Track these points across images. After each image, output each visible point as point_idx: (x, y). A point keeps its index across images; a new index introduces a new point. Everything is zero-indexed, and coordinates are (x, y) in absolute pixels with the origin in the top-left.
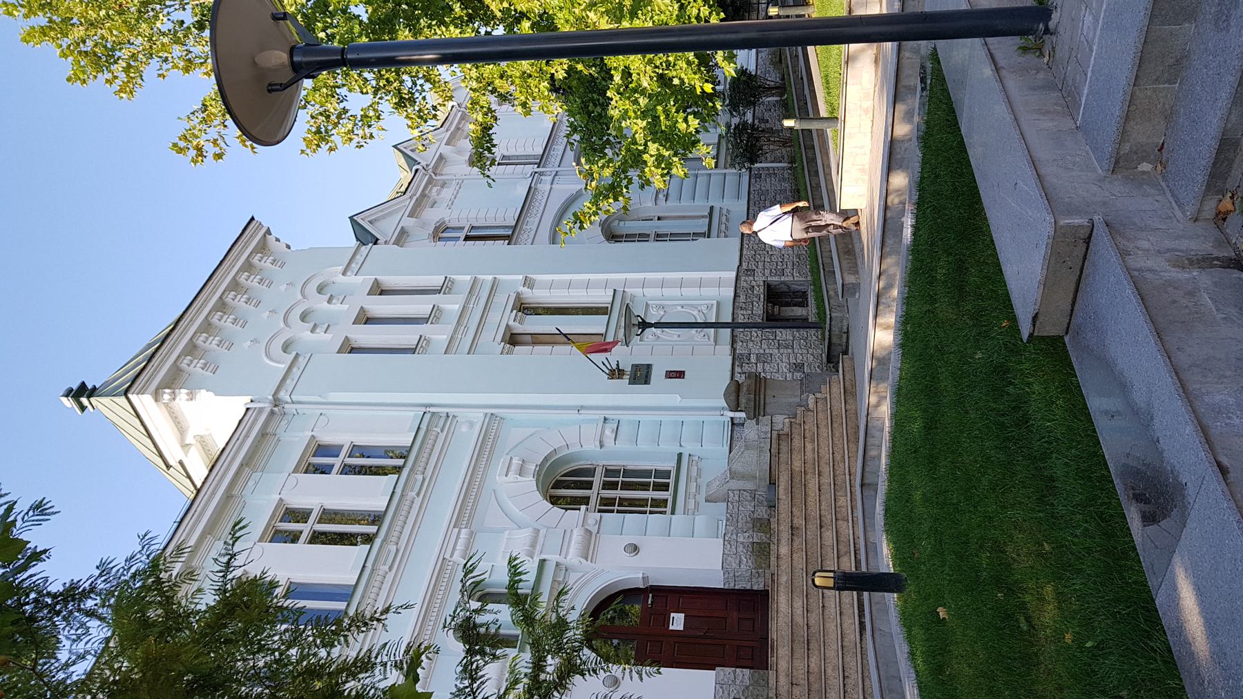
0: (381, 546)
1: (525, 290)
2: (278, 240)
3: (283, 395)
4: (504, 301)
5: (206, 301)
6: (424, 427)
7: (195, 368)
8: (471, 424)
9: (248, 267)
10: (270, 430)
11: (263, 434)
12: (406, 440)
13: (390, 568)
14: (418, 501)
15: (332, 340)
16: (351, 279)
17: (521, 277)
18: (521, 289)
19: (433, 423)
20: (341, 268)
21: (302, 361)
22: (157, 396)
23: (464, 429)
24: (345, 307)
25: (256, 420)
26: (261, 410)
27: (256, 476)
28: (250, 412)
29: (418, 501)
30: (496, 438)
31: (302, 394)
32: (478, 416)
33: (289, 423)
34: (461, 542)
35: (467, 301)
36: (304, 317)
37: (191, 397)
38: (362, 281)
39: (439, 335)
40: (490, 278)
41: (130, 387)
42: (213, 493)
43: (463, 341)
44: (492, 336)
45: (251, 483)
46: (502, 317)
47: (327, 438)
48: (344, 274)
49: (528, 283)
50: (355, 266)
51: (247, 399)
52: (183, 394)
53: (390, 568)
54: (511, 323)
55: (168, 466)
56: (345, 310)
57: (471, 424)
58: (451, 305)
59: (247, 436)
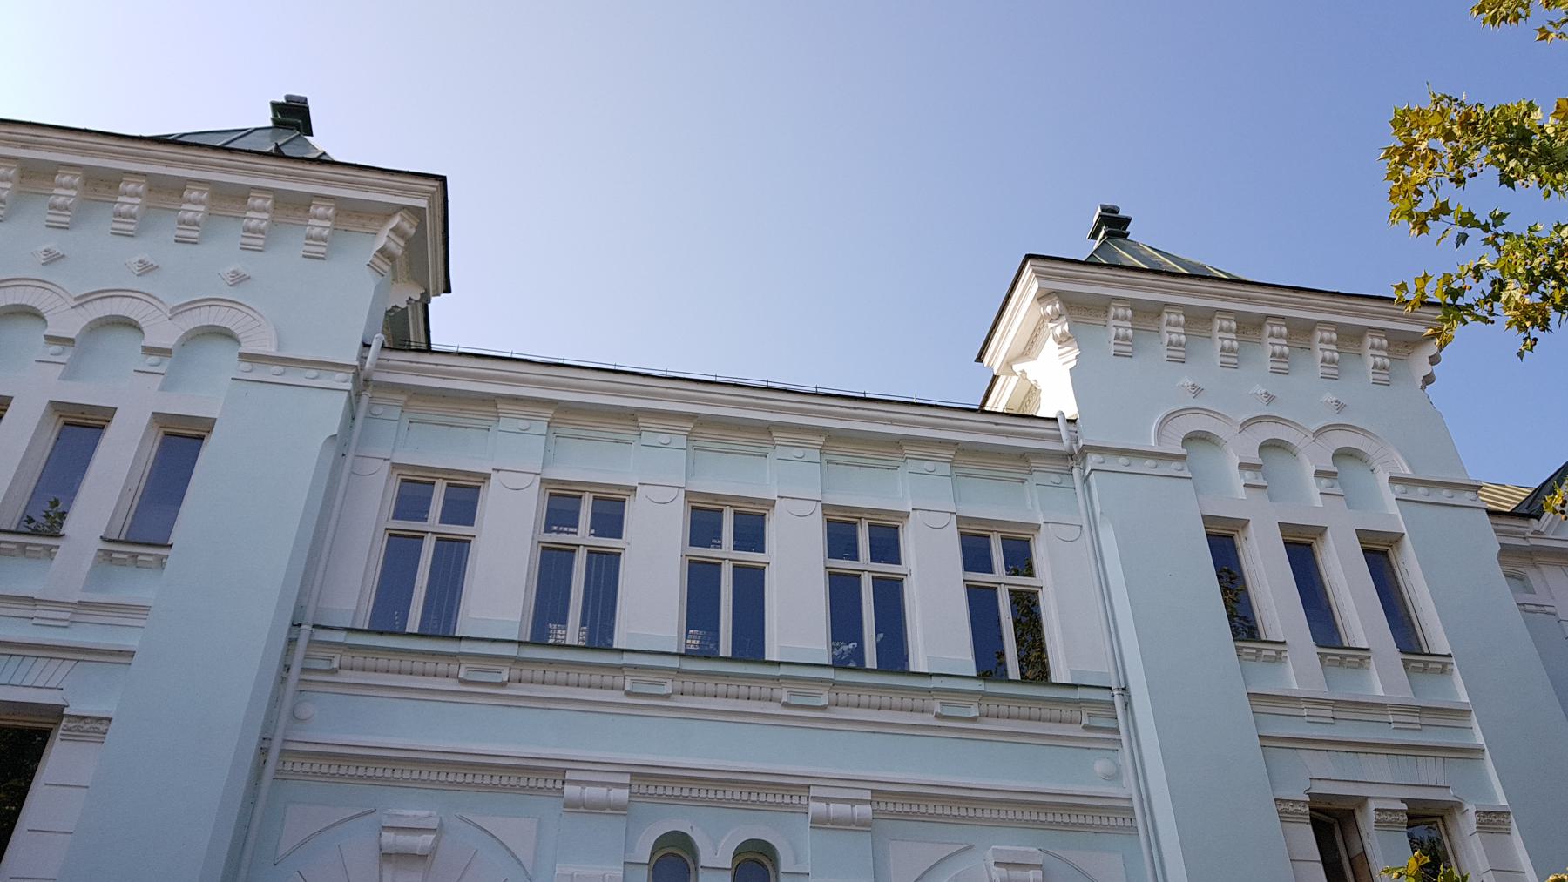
0: (822, 680)
1: (1472, 818)
2: (1434, 360)
3: (1093, 460)
4: (1430, 781)
5: (1249, 300)
6: (1080, 694)
7: (1118, 325)
8: (1114, 777)
9: (1301, 332)
10: (1034, 463)
11: (1024, 456)
12: (1060, 671)
13: (786, 705)
14: (928, 719)
15: (1233, 494)
16: (1389, 496)
17: (1502, 801)
18: (1471, 808)
19: (1100, 708)
20: (1406, 471)
21: (1173, 468)
22: (1043, 297)
23: (1101, 766)
24: (1318, 501)
25: (1042, 437)
26: (1059, 438)
27: (945, 469)
28: (1051, 425)
29: (928, 719)
30: (1096, 830)
31: (1106, 487)
32: (1127, 787)
33: (1057, 485)
34: (844, 809)
35: (1398, 708)
36: (1272, 446)
37: (1062, 341)
38: (1389, 514)
39: (1300, 669)
40: (1480, 740)
41: (1182, 275)
42: (892, 422)
43: (1276, 723)
44: (1331, 776)
45: (928, 466)
46: (1381, 786)
47: (773, 531)
48: (1319, 474)
49: (1492, 821)
50: (1420, 493)
51: (1071, 411)
52: (1062, 327)
53: (786, 705)
54: (1372, 805)
55: (980, 359)
56: (1311, 503)
57: (1114, 777)
58: (1384, 679)
59: (772, 409)
